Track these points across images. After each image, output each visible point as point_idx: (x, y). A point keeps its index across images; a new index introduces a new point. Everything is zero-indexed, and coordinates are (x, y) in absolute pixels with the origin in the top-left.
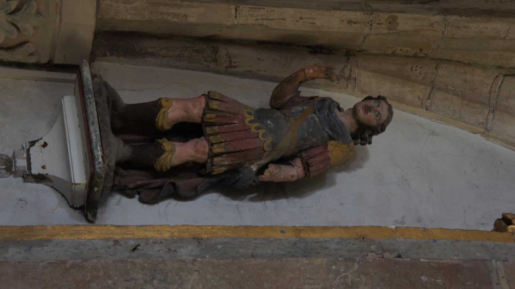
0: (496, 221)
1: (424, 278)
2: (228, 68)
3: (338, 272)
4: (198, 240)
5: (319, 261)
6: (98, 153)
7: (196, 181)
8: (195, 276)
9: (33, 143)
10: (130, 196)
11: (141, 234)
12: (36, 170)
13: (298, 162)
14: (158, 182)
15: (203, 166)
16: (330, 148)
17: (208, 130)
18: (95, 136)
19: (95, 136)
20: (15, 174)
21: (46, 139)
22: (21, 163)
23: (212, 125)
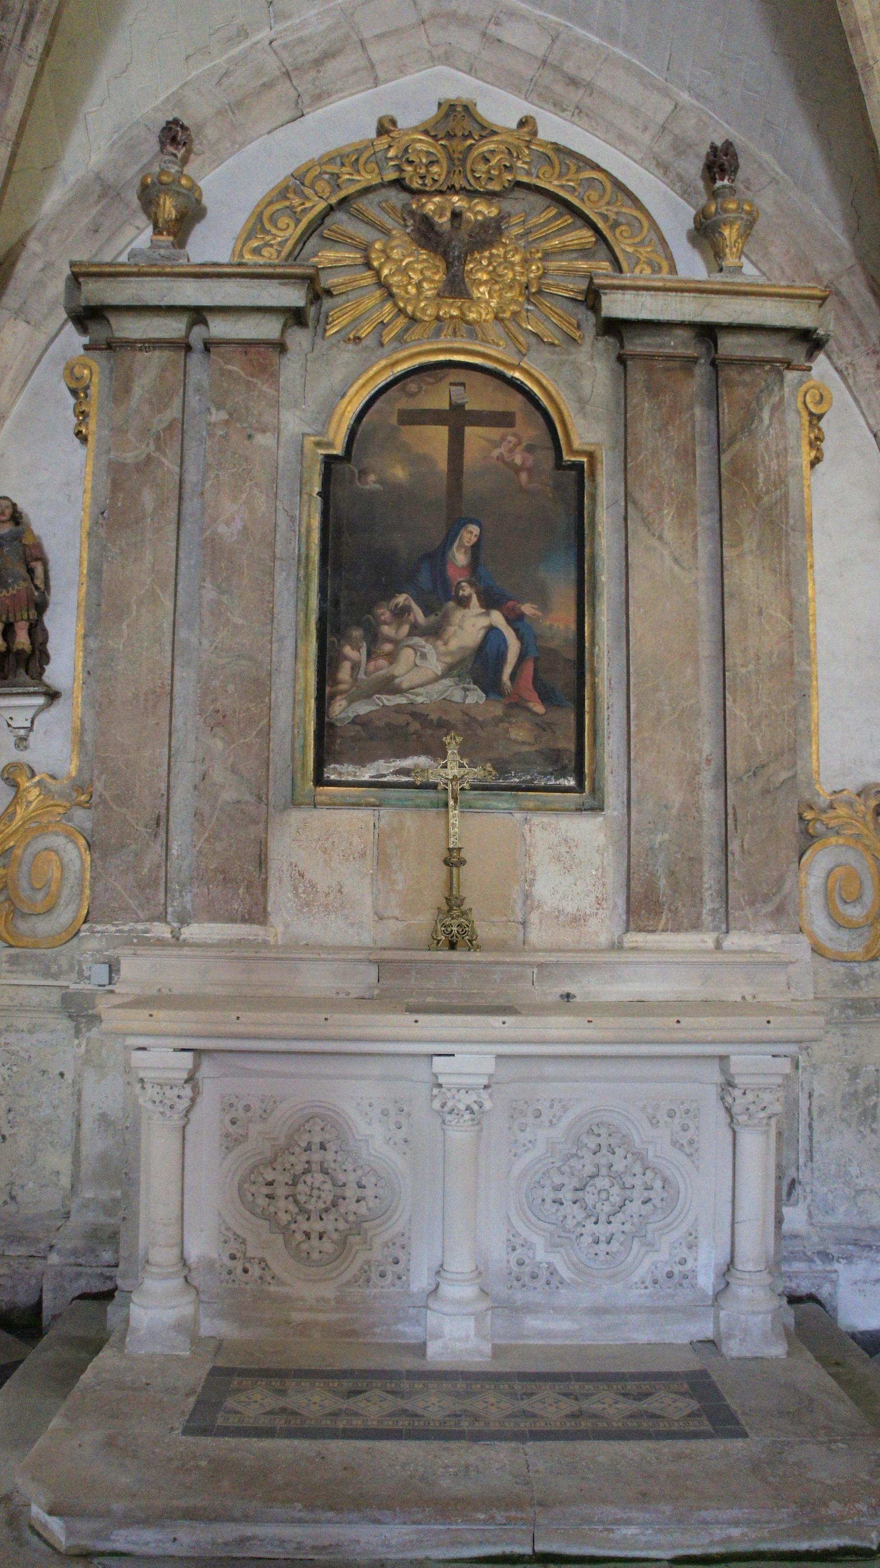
0: (500, 631)
1: (119, 504)
2: (824, 789)
3: (112, 557)
4: (85, 636)
5: (105, 567)
6: (31, 689)
7: (39, 629)
8: (110, 642)
9: (9, 725)
10: (43, 670)
11: (80, 668)
12: (28, 724)
13: (33, 564)
14: (37, 652)
15: (31, 624)
16: (26, 543)
17: (12, 620)
18: (20, 690)
19: (20, 690)
20: (28, 736)
21: (7, 718)
22: (22, 732)
23: (8, 618)
